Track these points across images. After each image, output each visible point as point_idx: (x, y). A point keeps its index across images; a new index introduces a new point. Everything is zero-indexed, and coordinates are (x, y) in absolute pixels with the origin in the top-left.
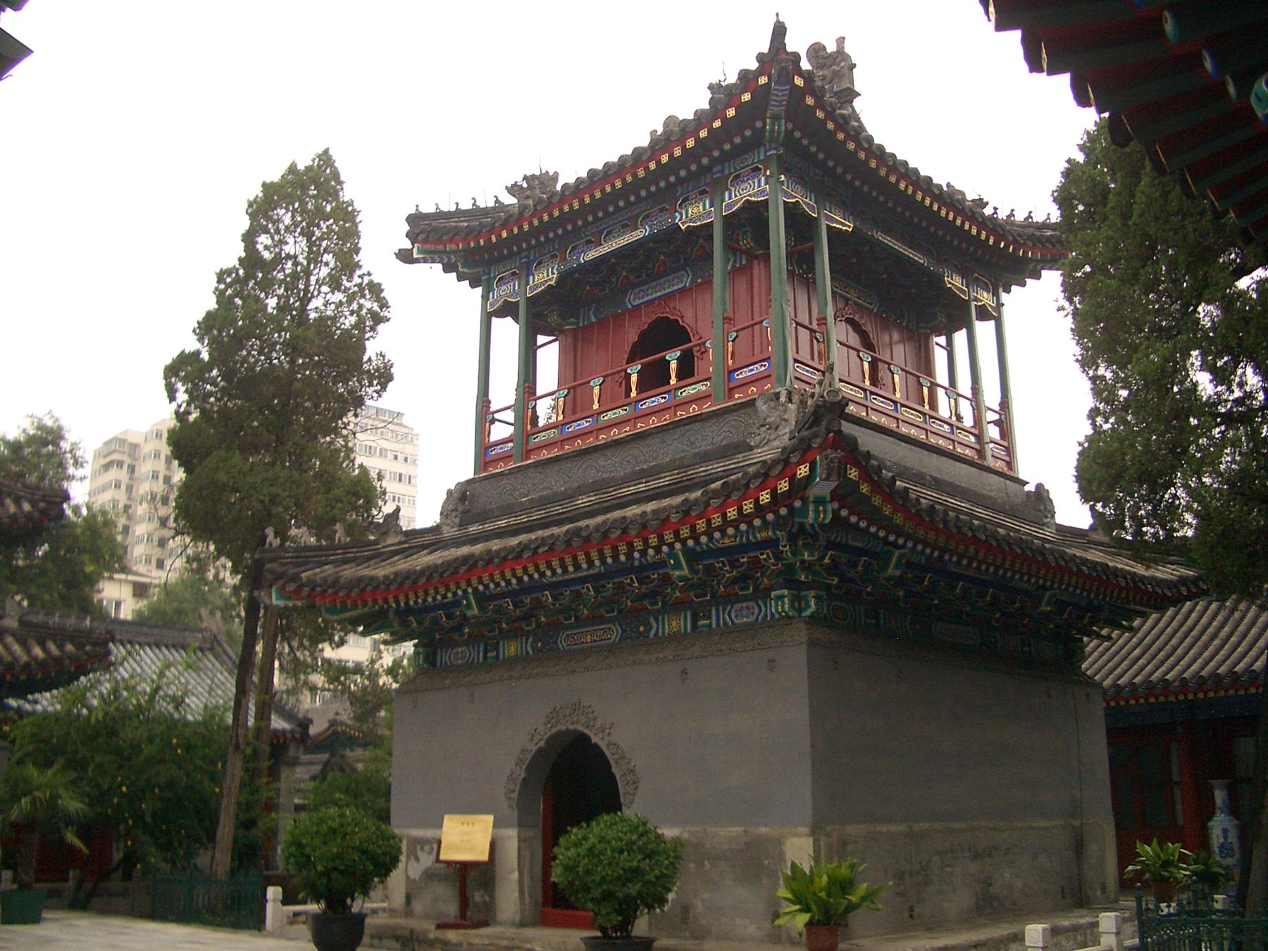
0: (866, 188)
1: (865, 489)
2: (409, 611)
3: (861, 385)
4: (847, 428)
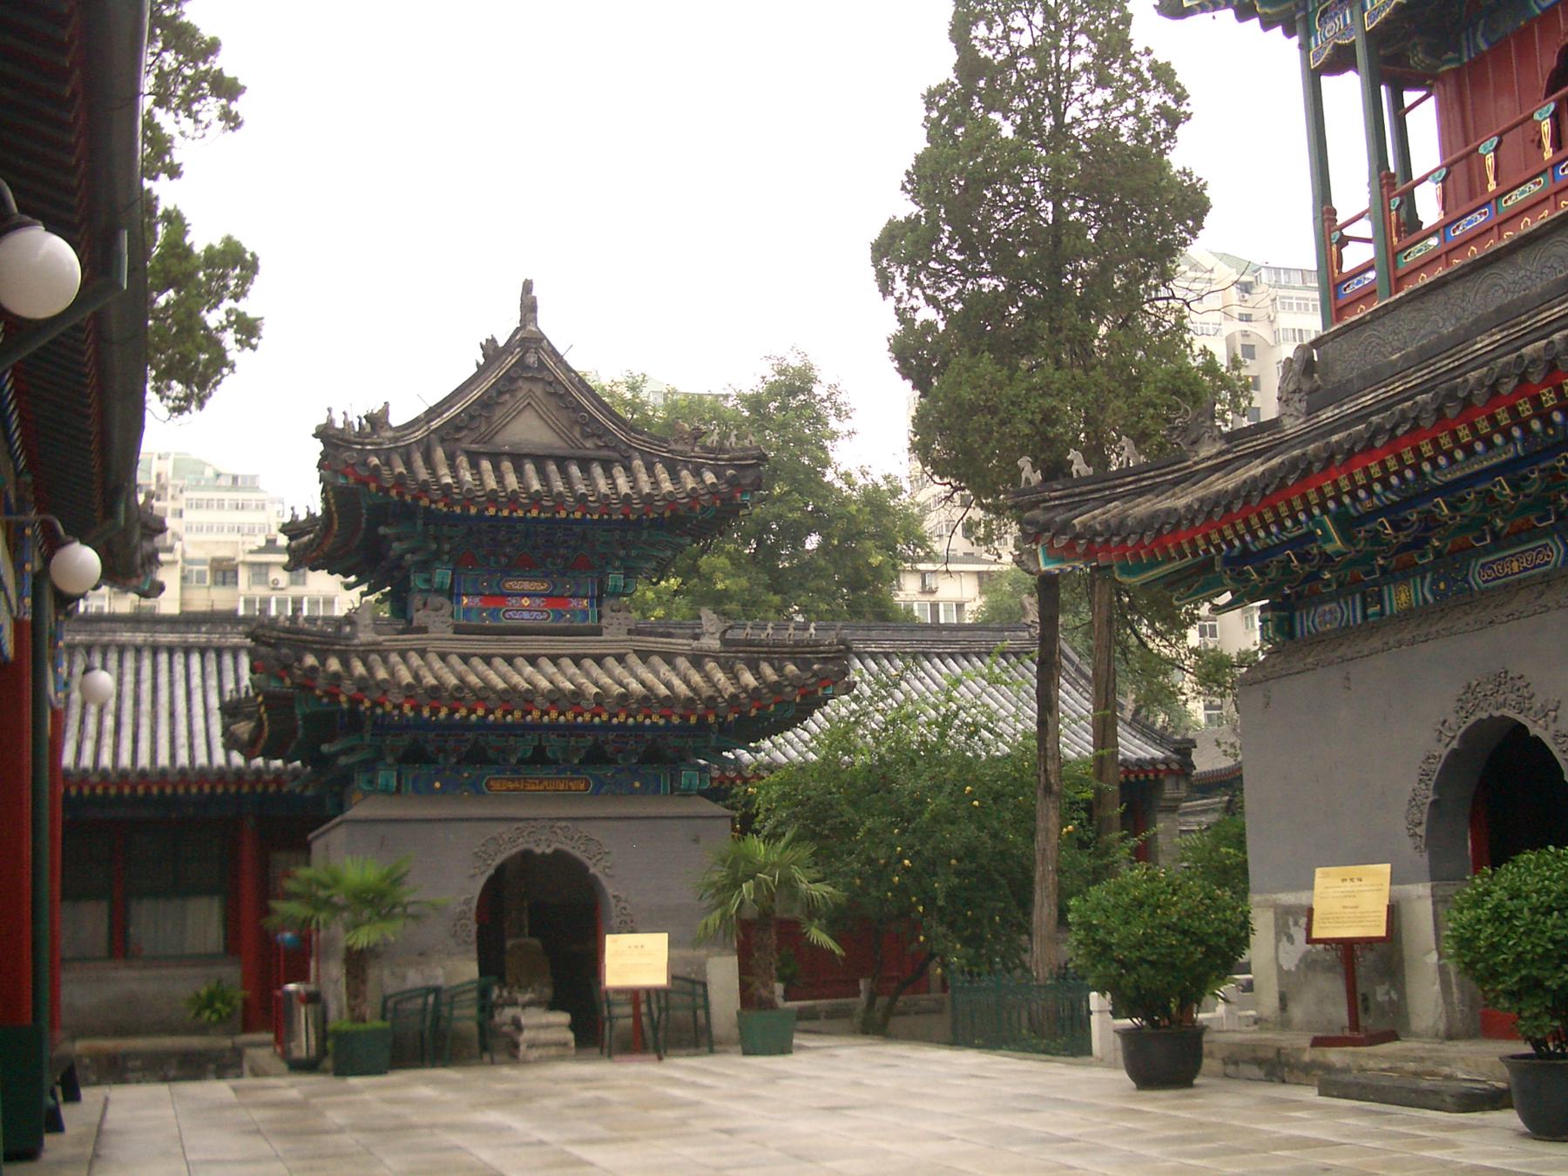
2: (1246, 555)
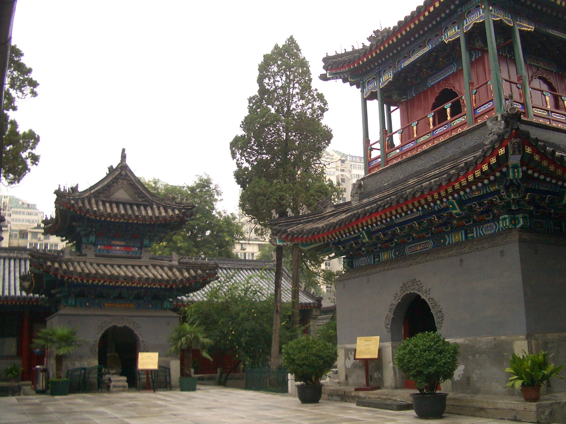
0: (539, 7)
1: (537, 158)
2: (340, 242)
3: (546, 108)
4: (523, 127)
